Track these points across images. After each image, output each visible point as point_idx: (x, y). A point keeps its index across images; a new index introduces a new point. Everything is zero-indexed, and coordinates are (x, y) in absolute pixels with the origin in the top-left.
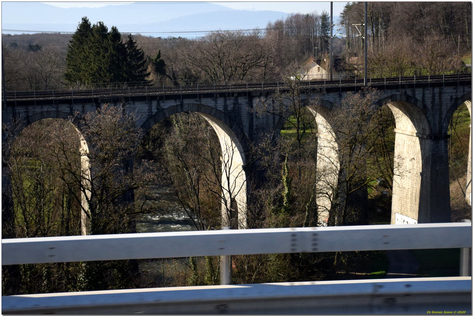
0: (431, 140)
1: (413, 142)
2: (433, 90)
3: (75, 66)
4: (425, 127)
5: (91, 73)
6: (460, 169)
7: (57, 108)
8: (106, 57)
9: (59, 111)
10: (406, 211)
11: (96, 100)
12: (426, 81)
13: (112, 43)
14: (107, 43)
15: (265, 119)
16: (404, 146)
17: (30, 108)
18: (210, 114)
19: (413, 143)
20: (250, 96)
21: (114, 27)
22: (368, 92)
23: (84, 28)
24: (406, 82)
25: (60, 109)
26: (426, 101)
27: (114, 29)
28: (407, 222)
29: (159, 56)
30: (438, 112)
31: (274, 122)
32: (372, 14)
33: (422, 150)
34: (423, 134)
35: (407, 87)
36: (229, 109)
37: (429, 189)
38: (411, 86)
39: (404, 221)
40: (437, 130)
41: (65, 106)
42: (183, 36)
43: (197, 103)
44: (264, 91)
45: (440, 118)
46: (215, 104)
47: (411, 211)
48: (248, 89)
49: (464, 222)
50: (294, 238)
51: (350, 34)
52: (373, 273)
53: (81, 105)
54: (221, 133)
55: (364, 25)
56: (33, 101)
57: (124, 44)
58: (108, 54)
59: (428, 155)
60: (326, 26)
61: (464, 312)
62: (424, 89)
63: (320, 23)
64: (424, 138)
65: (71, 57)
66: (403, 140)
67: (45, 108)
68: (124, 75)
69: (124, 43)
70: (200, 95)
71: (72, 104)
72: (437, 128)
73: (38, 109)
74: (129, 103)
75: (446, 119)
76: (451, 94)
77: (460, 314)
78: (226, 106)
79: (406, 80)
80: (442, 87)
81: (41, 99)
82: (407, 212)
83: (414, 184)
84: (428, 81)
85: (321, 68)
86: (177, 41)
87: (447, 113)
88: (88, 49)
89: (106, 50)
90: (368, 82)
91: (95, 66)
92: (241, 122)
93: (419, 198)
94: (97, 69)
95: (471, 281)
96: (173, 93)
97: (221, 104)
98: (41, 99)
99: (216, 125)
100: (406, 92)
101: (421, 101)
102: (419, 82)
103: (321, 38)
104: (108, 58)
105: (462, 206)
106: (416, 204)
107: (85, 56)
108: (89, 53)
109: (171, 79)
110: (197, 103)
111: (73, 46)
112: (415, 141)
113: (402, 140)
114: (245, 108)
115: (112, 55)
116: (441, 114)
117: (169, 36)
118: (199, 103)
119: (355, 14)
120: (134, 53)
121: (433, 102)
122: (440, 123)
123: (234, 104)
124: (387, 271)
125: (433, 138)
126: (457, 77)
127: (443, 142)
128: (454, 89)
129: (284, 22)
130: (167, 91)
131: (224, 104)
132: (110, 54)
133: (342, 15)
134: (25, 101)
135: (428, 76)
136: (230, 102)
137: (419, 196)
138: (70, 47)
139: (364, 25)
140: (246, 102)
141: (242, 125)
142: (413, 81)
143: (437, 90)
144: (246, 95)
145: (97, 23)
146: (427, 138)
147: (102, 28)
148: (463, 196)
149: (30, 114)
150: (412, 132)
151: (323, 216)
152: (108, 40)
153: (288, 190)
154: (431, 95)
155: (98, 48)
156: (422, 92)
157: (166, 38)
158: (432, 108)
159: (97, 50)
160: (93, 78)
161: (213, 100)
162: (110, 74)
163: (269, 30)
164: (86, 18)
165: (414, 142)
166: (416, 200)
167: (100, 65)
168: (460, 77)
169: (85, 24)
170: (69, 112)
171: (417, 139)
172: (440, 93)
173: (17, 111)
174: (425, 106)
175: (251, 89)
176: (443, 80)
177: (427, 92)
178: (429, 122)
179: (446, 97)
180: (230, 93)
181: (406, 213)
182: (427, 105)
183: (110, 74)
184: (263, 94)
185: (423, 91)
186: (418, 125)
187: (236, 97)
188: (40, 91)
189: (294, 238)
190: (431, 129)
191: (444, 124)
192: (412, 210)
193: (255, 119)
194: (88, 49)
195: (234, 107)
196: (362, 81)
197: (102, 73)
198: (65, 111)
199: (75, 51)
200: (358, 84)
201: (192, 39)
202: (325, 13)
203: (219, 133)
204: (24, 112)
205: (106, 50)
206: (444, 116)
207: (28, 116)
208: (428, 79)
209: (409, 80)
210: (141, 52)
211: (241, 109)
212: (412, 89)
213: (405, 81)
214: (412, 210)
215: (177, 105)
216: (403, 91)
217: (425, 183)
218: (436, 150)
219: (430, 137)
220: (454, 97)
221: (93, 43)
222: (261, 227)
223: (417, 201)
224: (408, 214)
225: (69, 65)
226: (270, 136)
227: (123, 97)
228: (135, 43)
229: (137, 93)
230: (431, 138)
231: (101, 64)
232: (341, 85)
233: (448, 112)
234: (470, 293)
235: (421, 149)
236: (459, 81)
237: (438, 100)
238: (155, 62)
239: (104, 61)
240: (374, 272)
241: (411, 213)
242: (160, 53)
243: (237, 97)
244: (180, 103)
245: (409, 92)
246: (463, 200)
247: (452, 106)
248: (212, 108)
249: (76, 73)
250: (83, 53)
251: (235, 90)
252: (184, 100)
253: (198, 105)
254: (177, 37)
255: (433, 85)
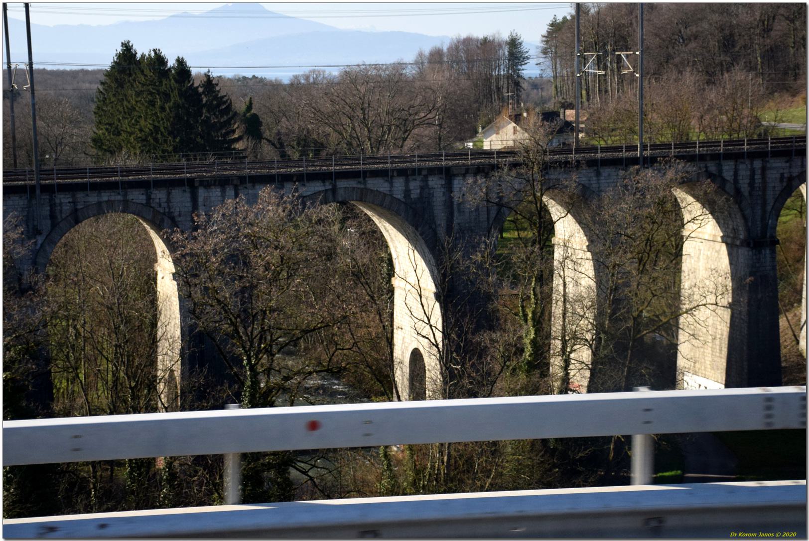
0: (747, 249)
1: (717, 251)
2: (752, 164)
3: (110, 125)
4: (737, 225)
5: (140, 137)
6: (785, 297)
7: (125, 195)
8: (168, 110)
9: (128, 201)
10: (703, 368)
11: (191, 182)
12: (740, 149)
13: (177, 85)
14: (168, 86)
15: (474, 214)
16: (698, 258)
17: (80, 196)
18: (381, 205)
19: (716, 254)
20: (448, 174)
21: (181, 57)
22: (670, 166)
23: (125, 61)
24: (707, 151)
25: (130, 197)
26: (741, 182)
27: (181, 62)
28: (706, 388)
29: (249, 108)
30: (759, 202)
31: (488, 219)
32: (596, 38)
33: (733, 266)
34: (734, 238)
35: (708, 158)
36: (412, 196)
37: (746, 332)
38: (716, 157)
39: (700, 385)
40: (759, 232)
41: (137, 193)
42: (260, 74)
43: (359, 186)
44: (472, 165)
45: (764, 211)
46: (389, 189)
47: (712, 368)
48: (444, 163)
49: (637, 390)
50: (769, 403)
51: (559, 70)
52: (661, 474)
53: (165, 191)
54: (394, 238)
55: (638, 53)
56: (85, 185)
57: (197, 87)
58: (171, 104)
59: (743, 273)
60: (517, 58)
61: (794, 534)
62: (737, 161)
63: (507, 53)
64: (737, 246)
65: (102, 110)
66: (697, 248)
67: (105, 196)
68: (199, 139)
69: (196, 85)
70: (365, 172)
71: (150, 188)
72: (759, 229)
73: (93, 198)
74: (246, 188)
75: (774, 212)
76: (781, 171)
77: (786, 538)
78: (407, 192)
79: (707, 147)
80: (767, 159)
81: (98, 180)
82: (705, 370)
83: (718, 323)
84: (744, 149)
85: (518, 128)
86: (251, 83)
87: (774, 204)
88: (134, 97)
89: (166, 96)
90: (644, 150)
91: (146, 125)
92: (434, 219)
93: (727, 346)
94: (150, 130)
95: (806, 486)
96: (320, 170)
97: (400, 188)
98: (98, 180)
99: (387, 225)
100: (706, 167)
101: (732, 182)
102: (729, 149)
103: (509, 77)
104: (171, 111)
105: (793, 359)
106: (721, 357)
107: (129, 106)
108: (137, 102)
109: (276, 147)
110: (359, 186)
111: (106, 90)
112: (720, 250)
113: (695, 248)
114: (439, 196)
115: (177, 106)
116: (764, 204)
117: (237, 73)
118: (362, 186)
119: (567, 37)
120: (215, 102)
121: (751, 184)
122: (763, 218)
123: (422, 188)
124: (685, 471)
125: (752, 245)
126: (791, 142)
127: (768, 252)
128: (787, 162)
129: (445, 49)
130: (309, 166)
131: (404, 188)
132: (174, 103)
133: (544, 39)
134: (77, 184)
135: (720, 142)
136: (415, 185)
137: (727, 342)
138: (101, 92)
139: (638, 53)
140: (442, 185)
141: (435, 223)
142: (719, 148)
143: (758, 164)
144: (441, 173)
145: (150, 52)
146: (742, 245)
147: (159, 60)
148: (794, 343)
149: (79, 207)
150: (715, 236)
151: (580, 377)
152: (170, 80)
153: (535, 334)
154: (749, 173)
155: (151, 94)
156: (733, 167)
157: (230, 77)
158: (750, 194)
159: (149, 97)
160: (144, 146)
161: (387, 181)
162: (174, 138)
163: (419, 63)
164: (129, 42)
165: (718, 252)
166: (721, 350)
167: (156, 123)
168: (797, 142)
169: (127, 53)
170: (144, 202)
171: (724, 246)
172: (764, 169)
173: (57, 201)
174: (738, 191)
175: (450, 163)
176: (768, 147)
177: (742, 167)
178: (744, 217)
179: (773, 176)
180: (415, 169)
181: (704, 372)
182: (742, 190)
183: (174, 138)
184: (470, 172)
185: (736, 166)
186: (724, 223)
187: (424, 176)
188: (43, 168)
189: (769, 403)
190: (748, 230)
191: (770, 221)
192: (715, 367)
193: (456, 214)
194: (134, 97)
195: (421, 193)
196: (635, 148)
197: (159, 136)
198: (137, 201)
199: (110, 100)
200: (627, 153)
201: (276, 80)
202: (514, 35)
203: (391, 239)
204: (69, 202)
205: (166, 96)
206: (769, 208)
207: (76, 210)
208: (744, 145)
209: (711, 146)
210: (227, 101)
211: (433, 196)
212: (717, 162)
213: (705, 149)
214: (715, 367)
215: (326, 191)
216: (702, 165)
217: (737, 320)
218: (757, 265)
219: (746, 243)
220: (786, 175)
221: (143, 85)
222: (490, 395)
223: (723, 353)
224: (707, 373)
225: (100, 123)
226: (491, 243)
227: (236, 176)
228: (217, 85)
229: (257, 169)
230: (748, 245)
231: (159, 122)
232: (599, 155)
233: (776, 201)
234: (804, 508)
235: (731, 264)
236: (794, 148)
237: (760, 181)
238: (243, 118)
239: (163, 116)
240: (663, 472)
241: (713, 372)
242: (251, 103)
243: (426, 176)
244: (330, 187)
245: (712, 168)
246: (795, 350)
247: (782, 191)
248: (385, 195)
249: (112, 136)
250: (125, 103)
251: (423, 164)
252: (337, 181)
253: (362, 189)
254: (250, 77)
255: (752, 156)
